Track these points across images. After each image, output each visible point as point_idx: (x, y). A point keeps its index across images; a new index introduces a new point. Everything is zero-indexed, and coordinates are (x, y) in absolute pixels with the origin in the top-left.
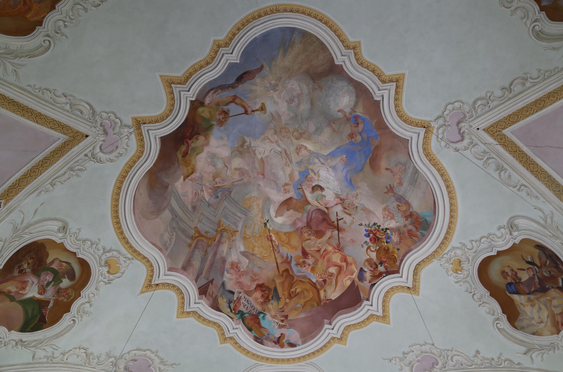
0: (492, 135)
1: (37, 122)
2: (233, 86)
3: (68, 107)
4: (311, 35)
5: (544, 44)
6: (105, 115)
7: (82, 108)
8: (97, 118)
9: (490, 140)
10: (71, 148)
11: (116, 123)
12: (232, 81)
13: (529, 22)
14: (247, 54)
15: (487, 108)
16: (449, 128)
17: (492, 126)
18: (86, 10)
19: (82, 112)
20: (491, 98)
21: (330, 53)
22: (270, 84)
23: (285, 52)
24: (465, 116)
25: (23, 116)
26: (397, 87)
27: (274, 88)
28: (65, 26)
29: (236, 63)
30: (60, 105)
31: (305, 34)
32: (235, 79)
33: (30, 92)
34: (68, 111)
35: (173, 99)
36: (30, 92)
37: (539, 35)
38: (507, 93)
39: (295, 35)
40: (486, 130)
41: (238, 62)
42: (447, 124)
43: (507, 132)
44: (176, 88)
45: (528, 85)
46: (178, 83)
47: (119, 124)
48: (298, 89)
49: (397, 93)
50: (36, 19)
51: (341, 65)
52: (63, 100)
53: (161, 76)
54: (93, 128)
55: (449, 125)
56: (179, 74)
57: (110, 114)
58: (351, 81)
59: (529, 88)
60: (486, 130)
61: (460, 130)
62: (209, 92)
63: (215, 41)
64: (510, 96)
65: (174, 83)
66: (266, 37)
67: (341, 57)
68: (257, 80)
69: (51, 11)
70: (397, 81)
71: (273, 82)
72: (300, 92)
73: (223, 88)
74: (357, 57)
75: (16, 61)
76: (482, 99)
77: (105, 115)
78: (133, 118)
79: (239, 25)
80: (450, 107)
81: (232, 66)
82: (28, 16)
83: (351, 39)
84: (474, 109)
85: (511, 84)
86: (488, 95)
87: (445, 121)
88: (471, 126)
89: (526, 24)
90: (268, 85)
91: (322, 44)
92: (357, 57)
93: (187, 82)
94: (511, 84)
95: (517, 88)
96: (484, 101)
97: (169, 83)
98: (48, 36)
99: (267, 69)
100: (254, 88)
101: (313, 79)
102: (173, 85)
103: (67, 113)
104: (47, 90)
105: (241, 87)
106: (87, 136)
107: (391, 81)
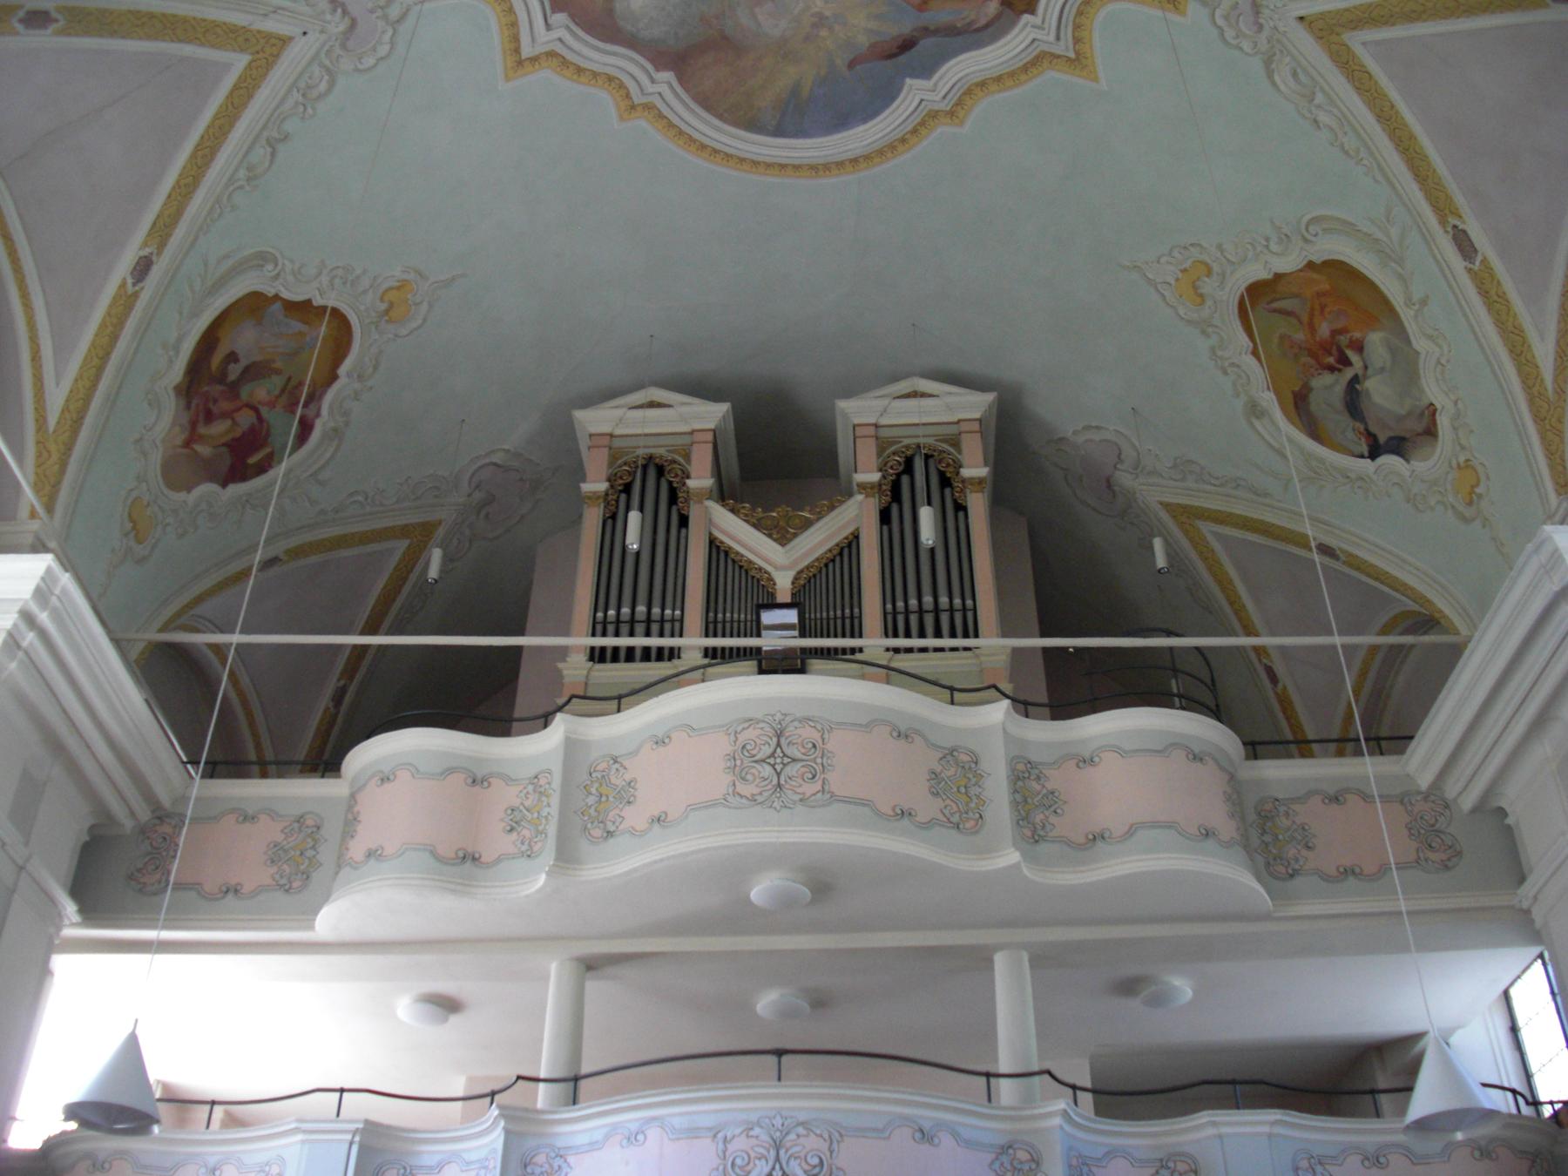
0: (268, 36)
1: (1393, 106)
2: (926, 31)
3: (1319, 98)
4: (736, 124)
5: (246, 253)
6: (1246, 46)
7: (1292, 83)
8: (1264, 46)
9: (271, 25)
10: (1347, 10)
11: (1226, 18)
12: (926, 44)
13: (289, 266)
14: (885, 95)
15: (302, 84)
16: (370, 5)
17: (277, 56)
18: (1220, 247)
19: (1295, 75)
20: (301, 109)
21: (687, 90)
22: (831, 29)
23: (795, 91)
24: (343, 46)
25: (1412, 137)
26: (517, 51)
27: (820, 21)
28: (1267, 239)
29: (913, 76)
30: (1335, 111)
31: (753, 125)
32: (918, 48)
33: (1381, 169)
34: (1322, 90)
35: (1077, 27)
36: (1381, 169)
37: (262, 258)
38: (275, 134)
39: (774, 123)
40: (285, 41)
41: (908, 81)
42: (379, 13)
43: (240, 61)
44: (1065, 48)
45: (242, 173)
46: (1059, 57)
47: (1218, 13)
48: (760, 17)
49: (516, 39)
50: (1315, 276)
51: (657, 70)
52: (1323, 118)
53: (1096, 80)
54: (1282, 29)
55: (372, 11)
56: (1052, 76)
57: (1234, 42)
58: (632, 42)
59: (236, 170)
60: (285, 41)
61: (345, 12)
62: (987, 26)
63: (962, 123)
64: (265, 134)
65: (1069, 59)
66: (842, 120)
67: (662, 86)
68: (863, 41)
69: (1284, 275)
70: (520, 63)
71: (824, 33)
72: (757, 10)
73: (951, 31)
74: (623, 92)
75: (1379, 235)
76: (321, 97)
77: (1246, 46)
78: (1183, 14)
79: (901, 148)
80: (383, 50)
81: (926, 71)
82: (1328, 287)
83: (642, 123)
84: (328, 71)
85: (273, 154)
86: (310, 111)
87: (385, 17)
88: (322, 32)
89: (292, 261)
90: (837, 27)
91: (708, 108)
92: (623, 92)
93: (1037, 57)
94: (273, 154)
95: (260, 152)
96: (314, 93)
97: (1078, 62)
98: (1306, 241)
99: (839, 62)
100: (873, 25)
101: (725, 38)
102: (1072, 55)
103: (1327, 88)
104: (1347, 153)
105: (905, 26)
106: (1302, 18)
107: (534, 60)
